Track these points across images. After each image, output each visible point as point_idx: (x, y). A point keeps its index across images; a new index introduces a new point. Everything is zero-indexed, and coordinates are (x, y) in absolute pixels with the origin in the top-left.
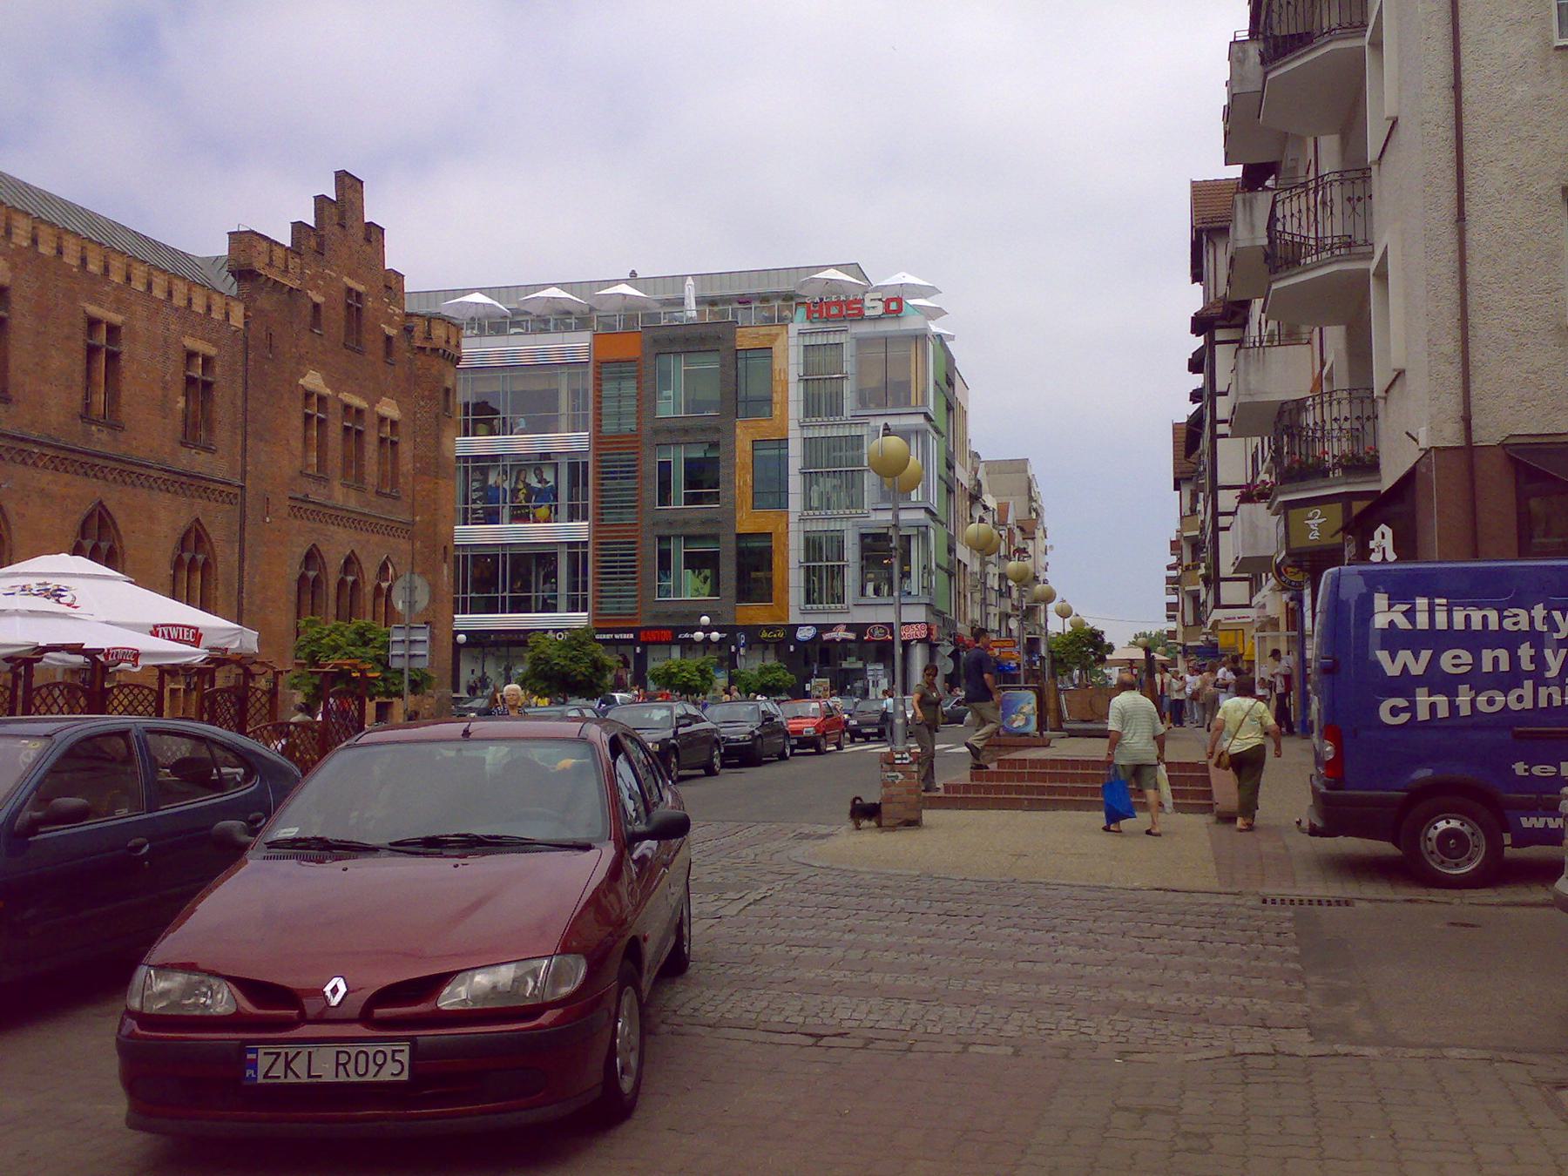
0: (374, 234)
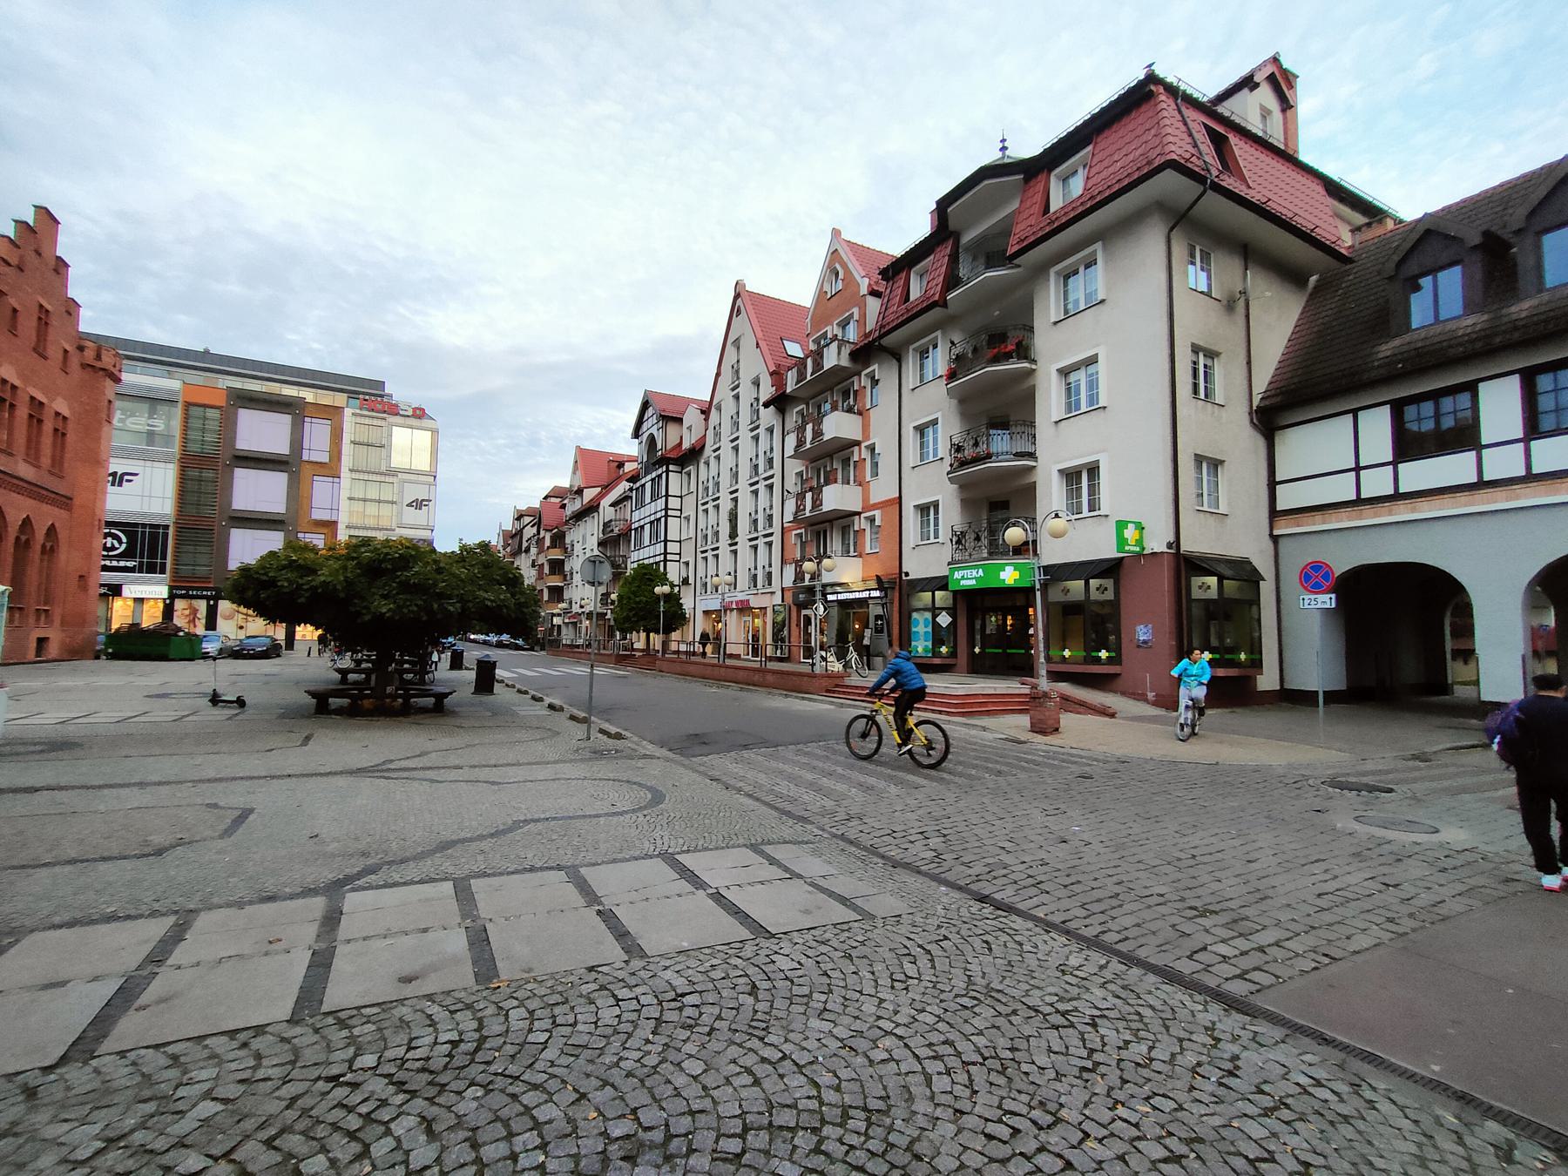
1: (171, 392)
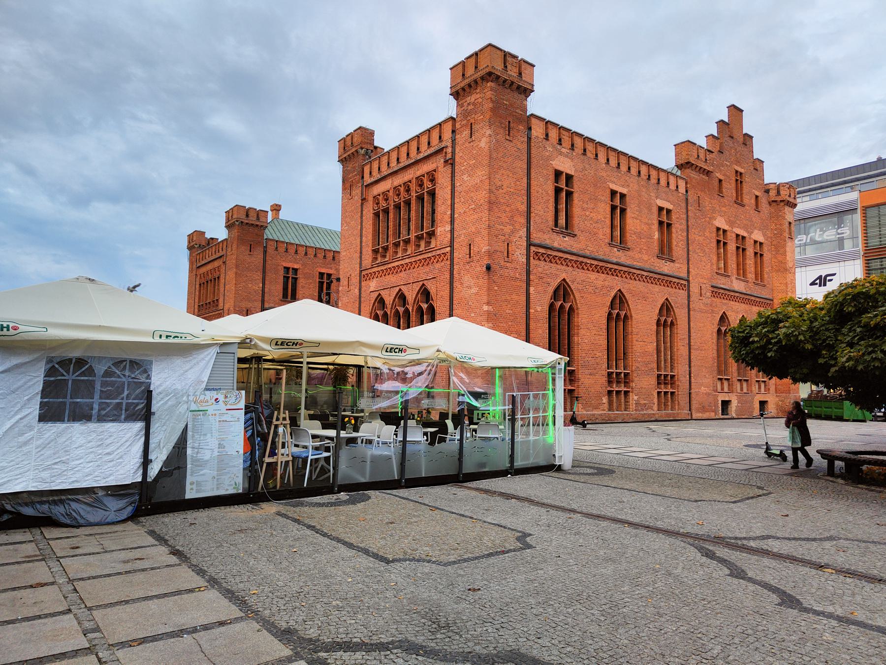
1: (852, 202)
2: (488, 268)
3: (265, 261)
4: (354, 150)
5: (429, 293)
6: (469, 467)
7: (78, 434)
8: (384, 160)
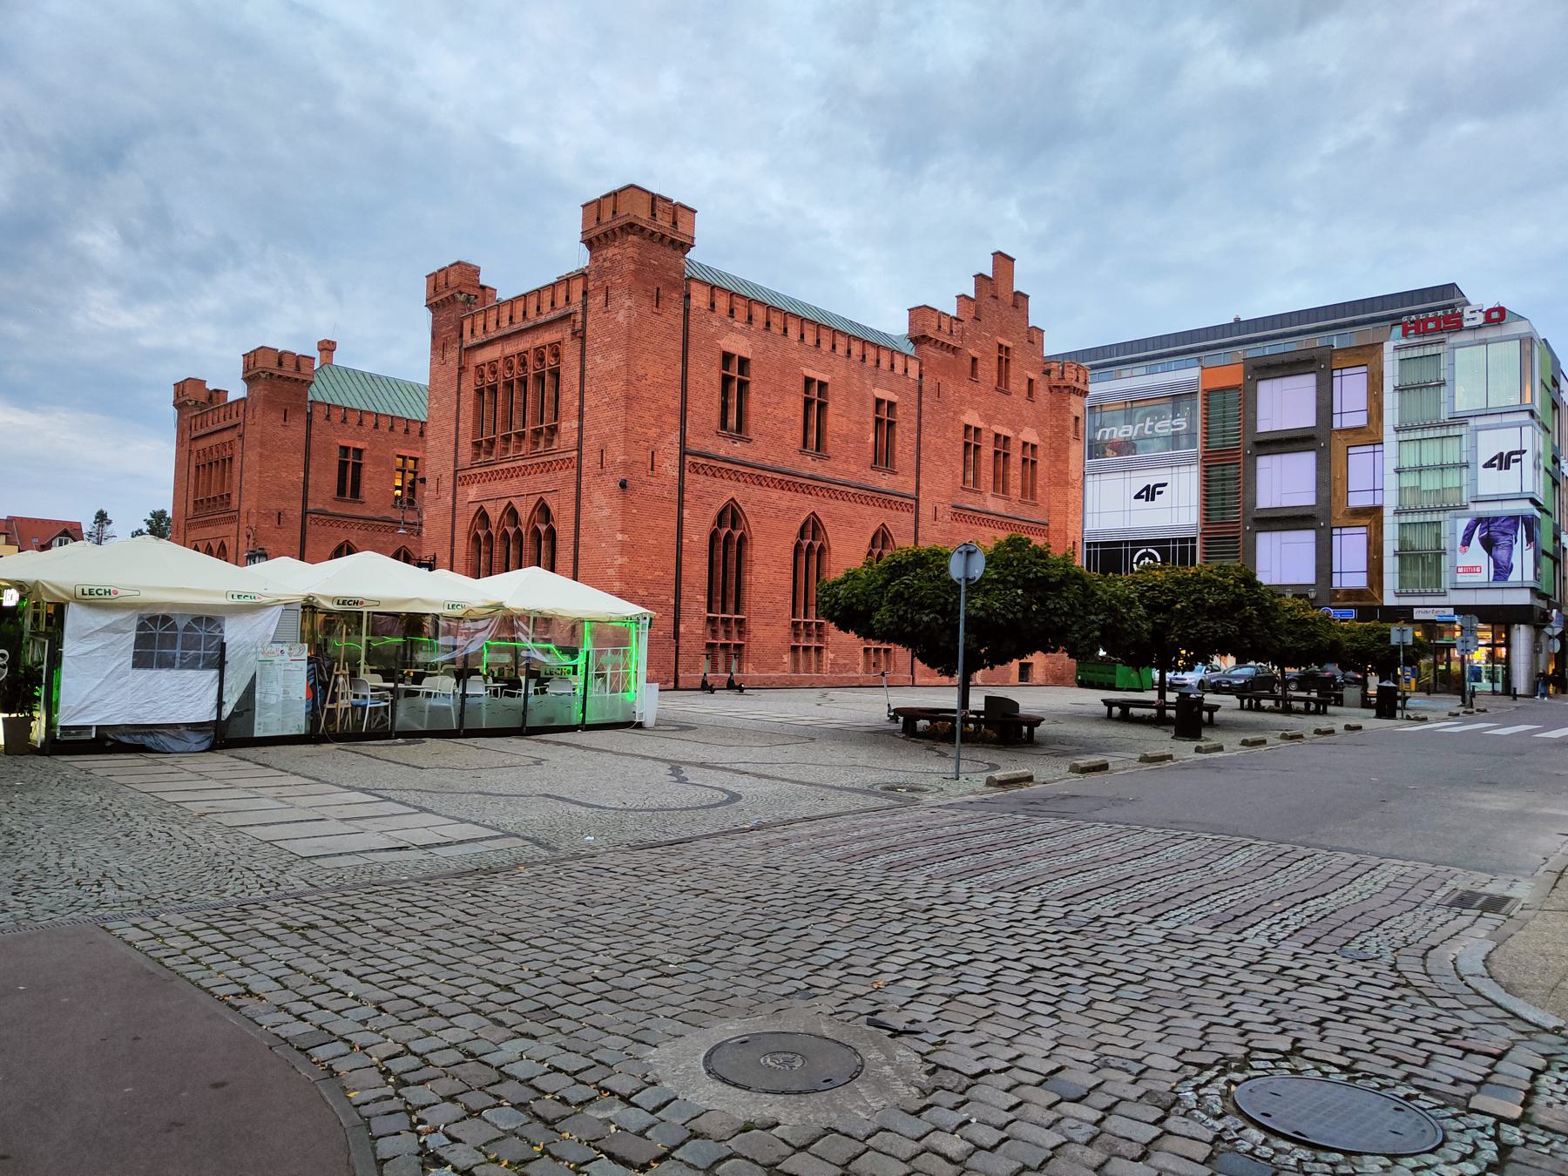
0: (1020, 299)
1: (1190, 383)
2: (623, 485)
3: (308, 436)
4: (449, 293)
5: (548, 511)
6: (533, 721)
7: (163, 680)
8: (493, 315)
